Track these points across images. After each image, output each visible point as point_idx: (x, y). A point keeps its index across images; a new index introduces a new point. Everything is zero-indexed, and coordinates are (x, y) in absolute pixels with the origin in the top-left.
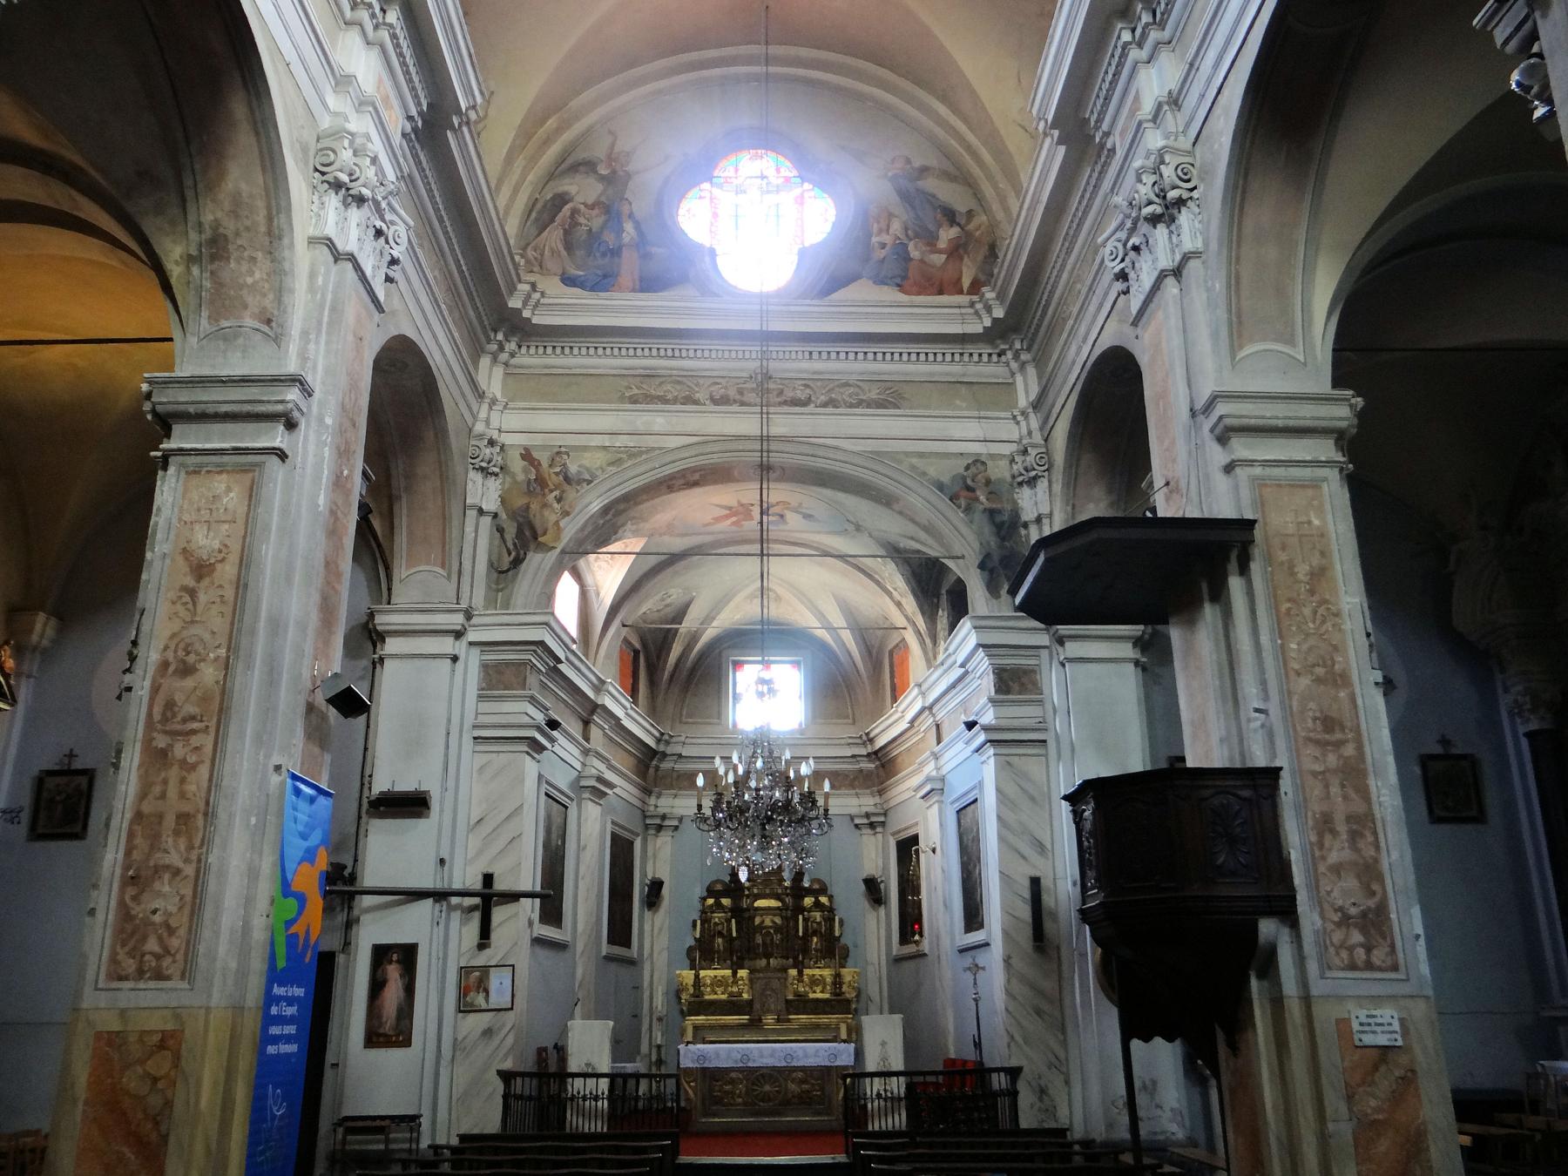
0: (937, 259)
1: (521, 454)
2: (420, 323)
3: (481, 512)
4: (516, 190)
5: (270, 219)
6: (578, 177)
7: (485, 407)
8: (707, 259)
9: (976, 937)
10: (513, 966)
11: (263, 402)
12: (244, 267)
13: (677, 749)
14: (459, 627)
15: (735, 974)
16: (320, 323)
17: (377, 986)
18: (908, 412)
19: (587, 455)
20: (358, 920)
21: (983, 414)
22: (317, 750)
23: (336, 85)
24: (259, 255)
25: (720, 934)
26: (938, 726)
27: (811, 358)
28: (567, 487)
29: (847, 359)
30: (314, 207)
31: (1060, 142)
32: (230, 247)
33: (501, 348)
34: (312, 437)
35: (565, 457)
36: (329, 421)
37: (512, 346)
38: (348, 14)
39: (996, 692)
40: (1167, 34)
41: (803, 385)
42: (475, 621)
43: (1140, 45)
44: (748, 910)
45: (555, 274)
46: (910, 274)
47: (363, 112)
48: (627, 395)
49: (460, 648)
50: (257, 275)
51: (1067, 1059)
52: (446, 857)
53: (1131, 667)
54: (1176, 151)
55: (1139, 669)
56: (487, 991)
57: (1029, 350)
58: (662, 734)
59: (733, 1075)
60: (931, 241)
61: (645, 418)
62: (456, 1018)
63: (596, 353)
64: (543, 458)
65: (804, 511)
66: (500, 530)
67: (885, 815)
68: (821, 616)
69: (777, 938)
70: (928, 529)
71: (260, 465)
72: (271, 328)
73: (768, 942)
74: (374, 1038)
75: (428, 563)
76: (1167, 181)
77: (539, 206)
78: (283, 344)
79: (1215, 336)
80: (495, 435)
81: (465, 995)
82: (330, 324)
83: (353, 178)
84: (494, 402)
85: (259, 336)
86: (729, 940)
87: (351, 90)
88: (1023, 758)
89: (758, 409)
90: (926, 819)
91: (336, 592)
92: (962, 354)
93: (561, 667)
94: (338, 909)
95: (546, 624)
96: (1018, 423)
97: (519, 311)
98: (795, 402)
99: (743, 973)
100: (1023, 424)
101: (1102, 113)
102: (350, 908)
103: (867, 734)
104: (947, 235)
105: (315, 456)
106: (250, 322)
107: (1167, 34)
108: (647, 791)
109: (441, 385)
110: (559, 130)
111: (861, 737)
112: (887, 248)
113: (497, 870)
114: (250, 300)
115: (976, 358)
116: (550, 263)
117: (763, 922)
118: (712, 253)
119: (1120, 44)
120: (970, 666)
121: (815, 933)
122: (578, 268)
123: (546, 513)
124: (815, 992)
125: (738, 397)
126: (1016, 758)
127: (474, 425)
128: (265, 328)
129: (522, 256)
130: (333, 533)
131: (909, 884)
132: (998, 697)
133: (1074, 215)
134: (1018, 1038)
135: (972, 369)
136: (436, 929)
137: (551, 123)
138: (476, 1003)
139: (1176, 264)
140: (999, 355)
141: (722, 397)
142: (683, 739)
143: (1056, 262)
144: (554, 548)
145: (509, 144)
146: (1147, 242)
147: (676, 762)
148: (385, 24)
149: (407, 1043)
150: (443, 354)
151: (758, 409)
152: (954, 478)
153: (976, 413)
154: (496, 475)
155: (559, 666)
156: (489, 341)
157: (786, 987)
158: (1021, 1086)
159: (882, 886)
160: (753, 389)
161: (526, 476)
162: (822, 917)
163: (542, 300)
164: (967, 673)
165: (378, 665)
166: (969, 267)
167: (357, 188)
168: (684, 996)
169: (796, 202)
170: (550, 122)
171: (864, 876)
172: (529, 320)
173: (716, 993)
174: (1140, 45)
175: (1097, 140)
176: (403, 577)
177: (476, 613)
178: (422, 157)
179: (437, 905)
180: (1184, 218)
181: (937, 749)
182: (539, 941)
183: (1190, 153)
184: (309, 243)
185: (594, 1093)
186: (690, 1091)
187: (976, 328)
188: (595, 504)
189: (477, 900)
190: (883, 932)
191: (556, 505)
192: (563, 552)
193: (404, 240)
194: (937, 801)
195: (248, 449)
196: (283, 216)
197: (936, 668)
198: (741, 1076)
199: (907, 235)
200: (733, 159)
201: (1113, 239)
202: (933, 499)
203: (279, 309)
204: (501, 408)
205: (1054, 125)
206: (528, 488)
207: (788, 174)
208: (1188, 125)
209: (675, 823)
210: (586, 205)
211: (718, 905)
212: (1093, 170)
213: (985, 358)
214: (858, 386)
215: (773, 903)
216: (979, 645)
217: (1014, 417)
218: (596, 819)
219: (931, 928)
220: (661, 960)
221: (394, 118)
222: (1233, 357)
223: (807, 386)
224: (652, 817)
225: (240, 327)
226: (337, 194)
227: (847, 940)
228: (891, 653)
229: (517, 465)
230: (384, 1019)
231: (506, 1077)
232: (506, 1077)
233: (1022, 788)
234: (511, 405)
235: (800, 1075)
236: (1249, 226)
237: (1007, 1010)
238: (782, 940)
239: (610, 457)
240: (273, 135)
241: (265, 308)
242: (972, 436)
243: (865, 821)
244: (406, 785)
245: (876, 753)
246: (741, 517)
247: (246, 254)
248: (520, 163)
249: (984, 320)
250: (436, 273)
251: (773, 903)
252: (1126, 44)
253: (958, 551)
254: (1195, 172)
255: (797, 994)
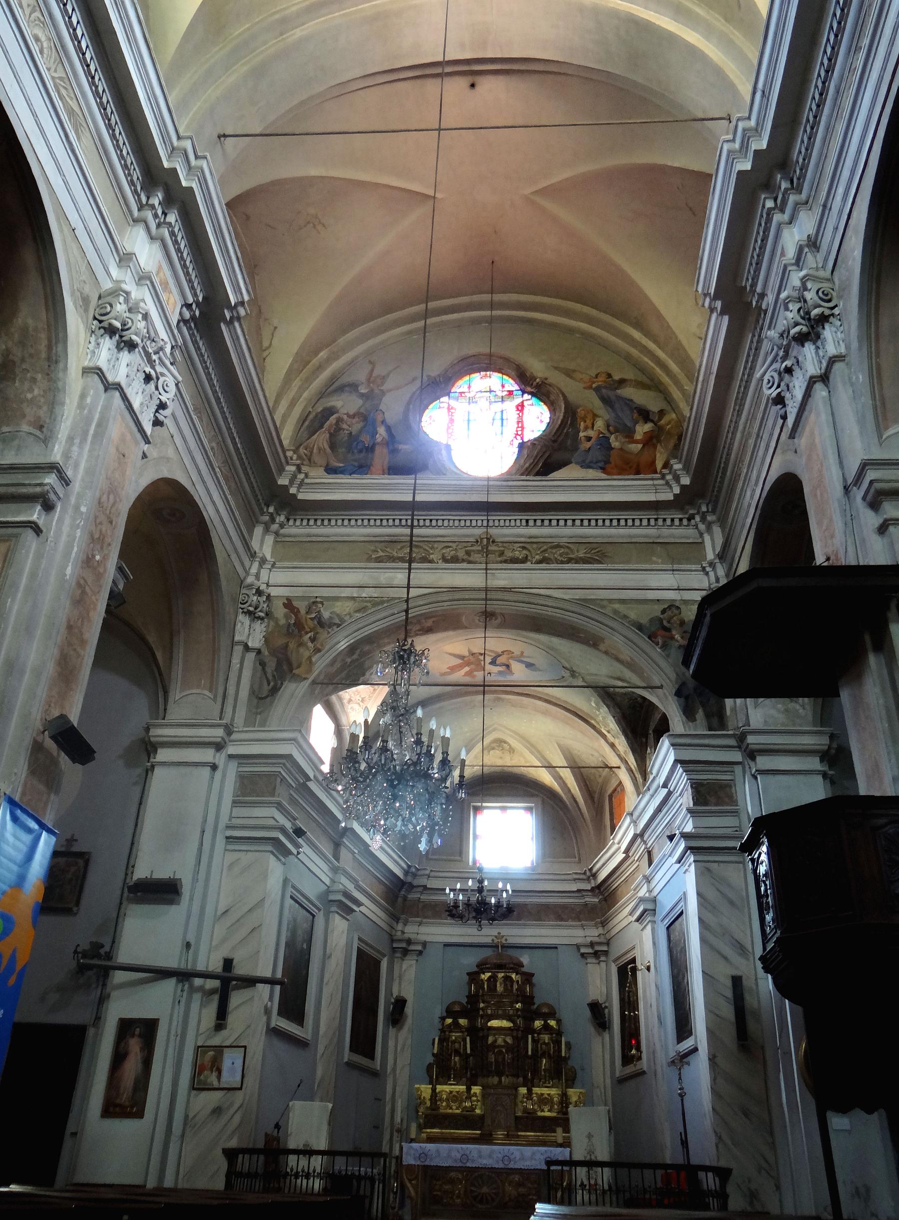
0: (636, 448)
1: (284, 604)
2: (195, 477)
3: (247, 648)
4: (292, 404)
5: (49, 347)
6: (344, 396)
7: (256, 565)
8: (444, 452)
9: (688, 1044)
10: (245, 1047)
11: (24, 485)
12: (27, 385)
13: (423, 881)
14: (219, 740)
15: (469, 1089)
16: (85, 433)
17: (119, 1058)
18: (610, 566)
19: (339, 604)
20: (109, 996)
21: (676, 567)
22: (42, 787)
23: (120, 261)
24: (39, 376)
25: (457, 1052)
26: (649, 853)
27: (527, 525)
28: (320, 630)
29: (558, 525)
30: (91, 346)
31: (723, 313)
32: (17, 370)
33: (273, 520)
34: (67, 521)
35: (320, 605)
36: (83, 509)
37: (282, 518)
38: (136, 213)
39: (694, 805)
40: (804, 196)
41: (520, 547)
42: (234, 736)
43: (782, 211)
44: (482, 1029)
45: (321, 466)
46: (612, 460)
47: (142, 285)
48: (373, 556)
49: (220, 759)
50: (36, 392)
51: (777, 1163)
52: (192, 942)
53: (819, 779)
54: (816, 279)
55: (828, 781)
56: (220, 1072)
57: (714, 512)
58: (409, 867)
59: (453, 1174)
60: (629, 434)
61: (387, 575)
62: (189, 1095)
63: (349, 523)
64: (302, 606)
65: (525, 660)
66: (263, 664)
67: (608, 944)
68: (541, 756)
69: (508, 1057)
70: (630, 665)
71: (17, 536)
72: (43, 432)
73: (500, 1060)
74: (112, 1110)
75: (198, 686)
76: (810, 303)
77: (311, 417)
78: (50, 445)
79: (861, 422)
80: (263, 587)
81: (200, 1074)
82: (95, 435)
83: (126, 327)
84: (263, 561)
85: (32, 438)
86: (465, 1057)
87: (131, 265)
88: (722, 864)
89: (483, 566)
90: (641, 941)
91: (79, 656)
92: (656, 520)
93: (310, 784)
94: (94, 986)
95: (294, 740)
96: (707, 574)
97: (286, 488)
98: (514, 560)
99: (476, 1089)
100: (712, 574)
101: (755, 278)
102: (104, 985)
103: (591, 870)
104: (642, 429)
105: (68, 536)
106: (25, 428)
107: (804, 196)
108: (394, 917)
109: (213, 534)
110: (329, 360)
111: (585, 873)
112: (593, 440)
113: (238, 958)
114: (27, 410)
115: (669, 522)
116: (316, 458)
117: (495, 1041)
118: (448, 447)
119: (765, 211)
120: (671, 785)
121: (543, 1055)
122: (340, 462)
123: (301, 650)
124: (543, 1111)
125: (466, 557)
126: (715, 865)
127: (245, 578)
128: (38, 433)
129: (295, 452)
130: (80, 599)
131: (629, 1001)
132: (695, 808)
133: (742, 380)
134: (725, 1137)
135: (665, 531)
136: (177, 1007)
137: (323, 354)
138: (209, 1080)
139: (823, 371)
140: (689, 520)
141: (452, 557)
142: (427, 872)
143: (730, 427)
144: (305, 679)
145: (287, 367)
146: (798, 362)
147: (422, 893)
148: (165, 223)
149: (140, 1115)
150: (217, 511)
151: (483, 566)
152: (652, 620)
153: (669, 567)
154: (262, 619)
155: (308, 783)
156: (262, 513)
157: (516, 1104)
158: (730, 1189)
159: (606, 1011)
160: (478, 550)
161: (287, 620)
162: (551, 1039)
163: (306, 481)
164: (669, 794)
165: (149, 772)
166: (661, 453)
167: (128, 336)
168: (422, 1110)
169: (518, 410)
170: (322, 354)
171: (589, 1001)
172: (294, 496)
173: (451, 1108)
174: (782, 211)
175: (754, 303)
176: (177, 698)
177: (235, 729)
178: (201, 344)
179: (180, 985)
180: (828, 332)
181: (648, 872)
182: (275, 1032)
183: (830, 280)
184: (83, 372)
185: (306, 1170)
186: (411, 1189)
187: (667, 496)
188: (342, 643)
189: (216, 983)
190: (607, 1057)
191: (310, 644)
192: (314, 683)
193: (172, 389)
194: (649, 921)
195: (8, 522)
196: (60, 347)
197: (644, 794)
198: (460, 1176)
199: (609, 430)
200: (467, 378)
201: (769, 371)
202: (631, 635)
203: (50, 418)
204: (270, 567)
205: (716, 297)
206: (288, 630)
207: (511, 389)
208: (826, 260)
209: (419, 948)
210: (347, 414)
211: (456, 1024)
212: (754, 336)
213: (677, 522)
214: (568, 547)
215: (505, 1024)
216: (676, 761)
217: (704, 569)
218: (343, 932)
219: (648, 1047)
220: (403, 1076)
221: (172, 301)
222: (880, 436)
223: (524, 548)
224: (400, 941)
225: (17, 431)
226: (111, 338)
227: (574, 1062)
228: (611, 797)
229: (280, 612)
230: (121, 1092)
231: (231, 1154)
232: (231, 1154)
233: (721, 892)
234: (278, 564)
235: (517, 1178)
236: (885, 323)
237: (713, 1109)
238: (513, 1059)
239: (357, 605)
240: (55, 277)
241: (39, 417)
242: (665, 585)
243: (590, 950)
244: (163, 873)
245: (599, 887)
246: (472, 666)
247: (29, 375)
248: (296, 384)
249: (674, 489)
250: (214, 444)
251: (505, 1024)
252: (770, 209)
253: (656, 681)
254: (834, 294)
255: (525, 1110)
